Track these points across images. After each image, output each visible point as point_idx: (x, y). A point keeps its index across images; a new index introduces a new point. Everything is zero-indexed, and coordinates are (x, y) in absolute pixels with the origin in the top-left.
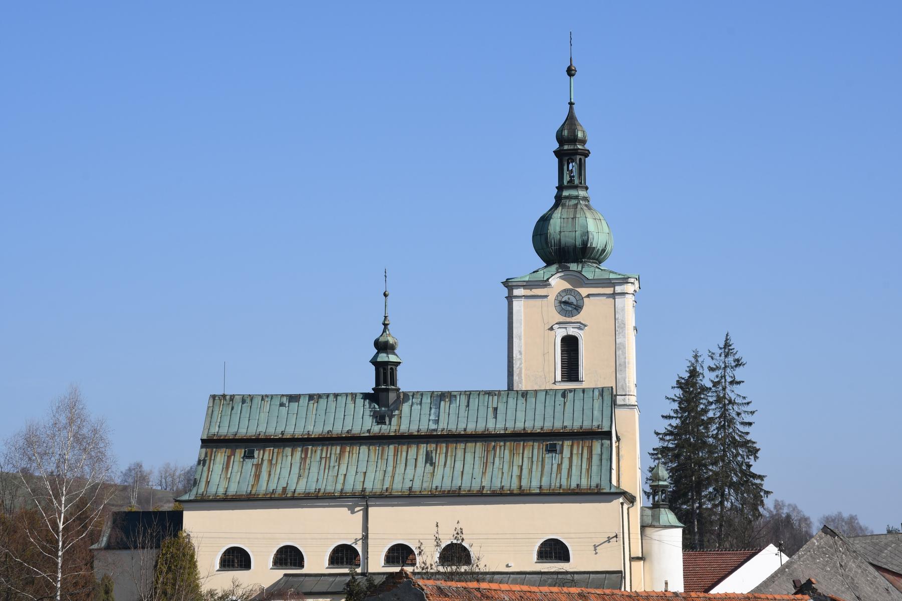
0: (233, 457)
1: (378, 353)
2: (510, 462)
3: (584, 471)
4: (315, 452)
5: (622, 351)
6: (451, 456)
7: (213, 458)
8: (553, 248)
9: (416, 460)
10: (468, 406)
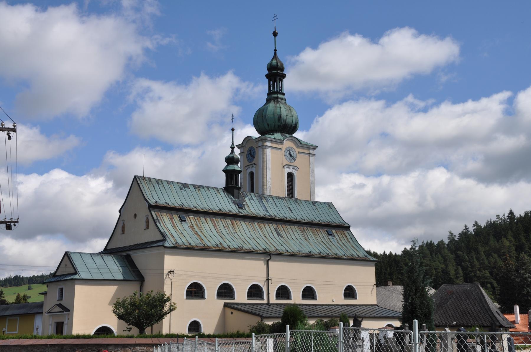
0: (173, 219)
1: (227, 166)
2: (316, 239)
3: (351, 247)
4: (218, 222)
5: (313, 185)
6: (288, 233)
7: (162, 219)
8: (282, 123)
9: (272, 233)
10: (275, 204)
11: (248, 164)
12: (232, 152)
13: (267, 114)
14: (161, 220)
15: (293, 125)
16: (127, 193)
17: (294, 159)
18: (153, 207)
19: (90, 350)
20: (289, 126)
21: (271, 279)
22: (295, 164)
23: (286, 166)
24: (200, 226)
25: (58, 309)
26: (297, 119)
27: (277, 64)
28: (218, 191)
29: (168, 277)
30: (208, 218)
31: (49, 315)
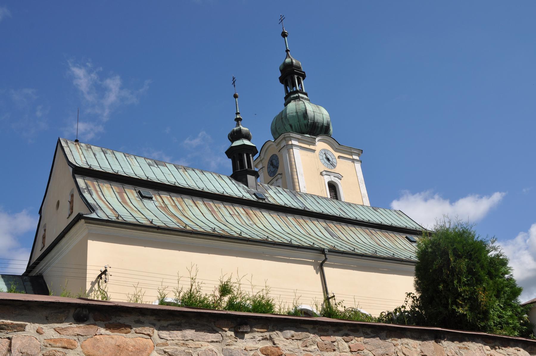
0: (125, 195)
4: (220, 208)
6: (347, 234)
8: (310, 121)
9: (320, 231)
10: (319, 203)
11: (271, 178)
13: (287, 113)
14: (97, 191)
16: (50, 173)
17: (334, 166)
18: (79, 171)
20: (320, 126)
21: (334, 296)
22: (336, 170)
23: (324, 173)
24: (181, 208)
27: (292, 61)
28: (220, 177)
29: (96, 286)
30: (199, 202)
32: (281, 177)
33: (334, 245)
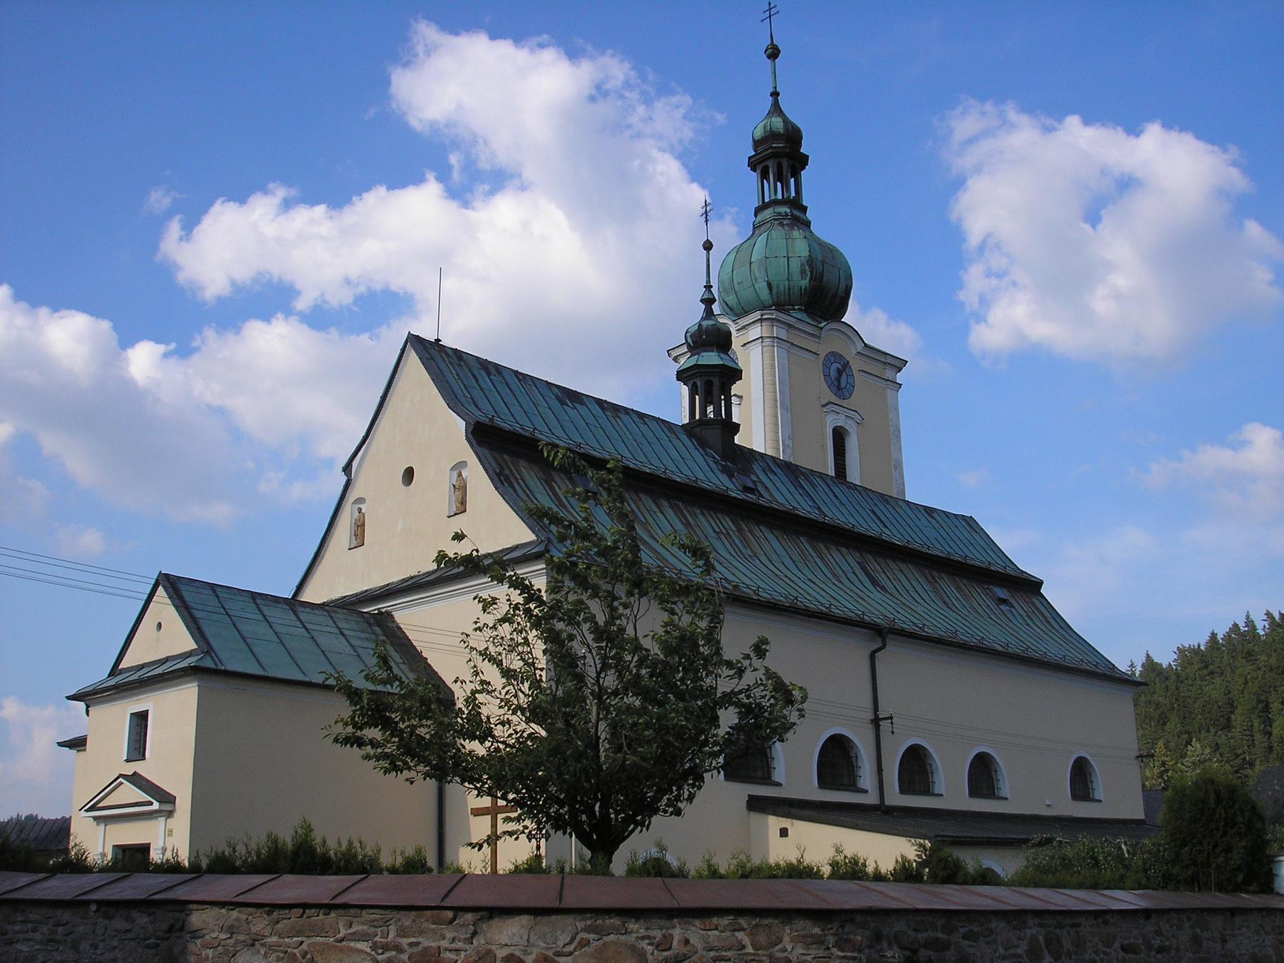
9: (854, 573)
12: (709, 313)
14: (517, 480)
15: (839, 294)
19: (364, 946)
21: (891, 718)
25: (130, 793)
26: (849, 277)
31: (95, 818)
32: (740, 404)
33: (894, 617)
